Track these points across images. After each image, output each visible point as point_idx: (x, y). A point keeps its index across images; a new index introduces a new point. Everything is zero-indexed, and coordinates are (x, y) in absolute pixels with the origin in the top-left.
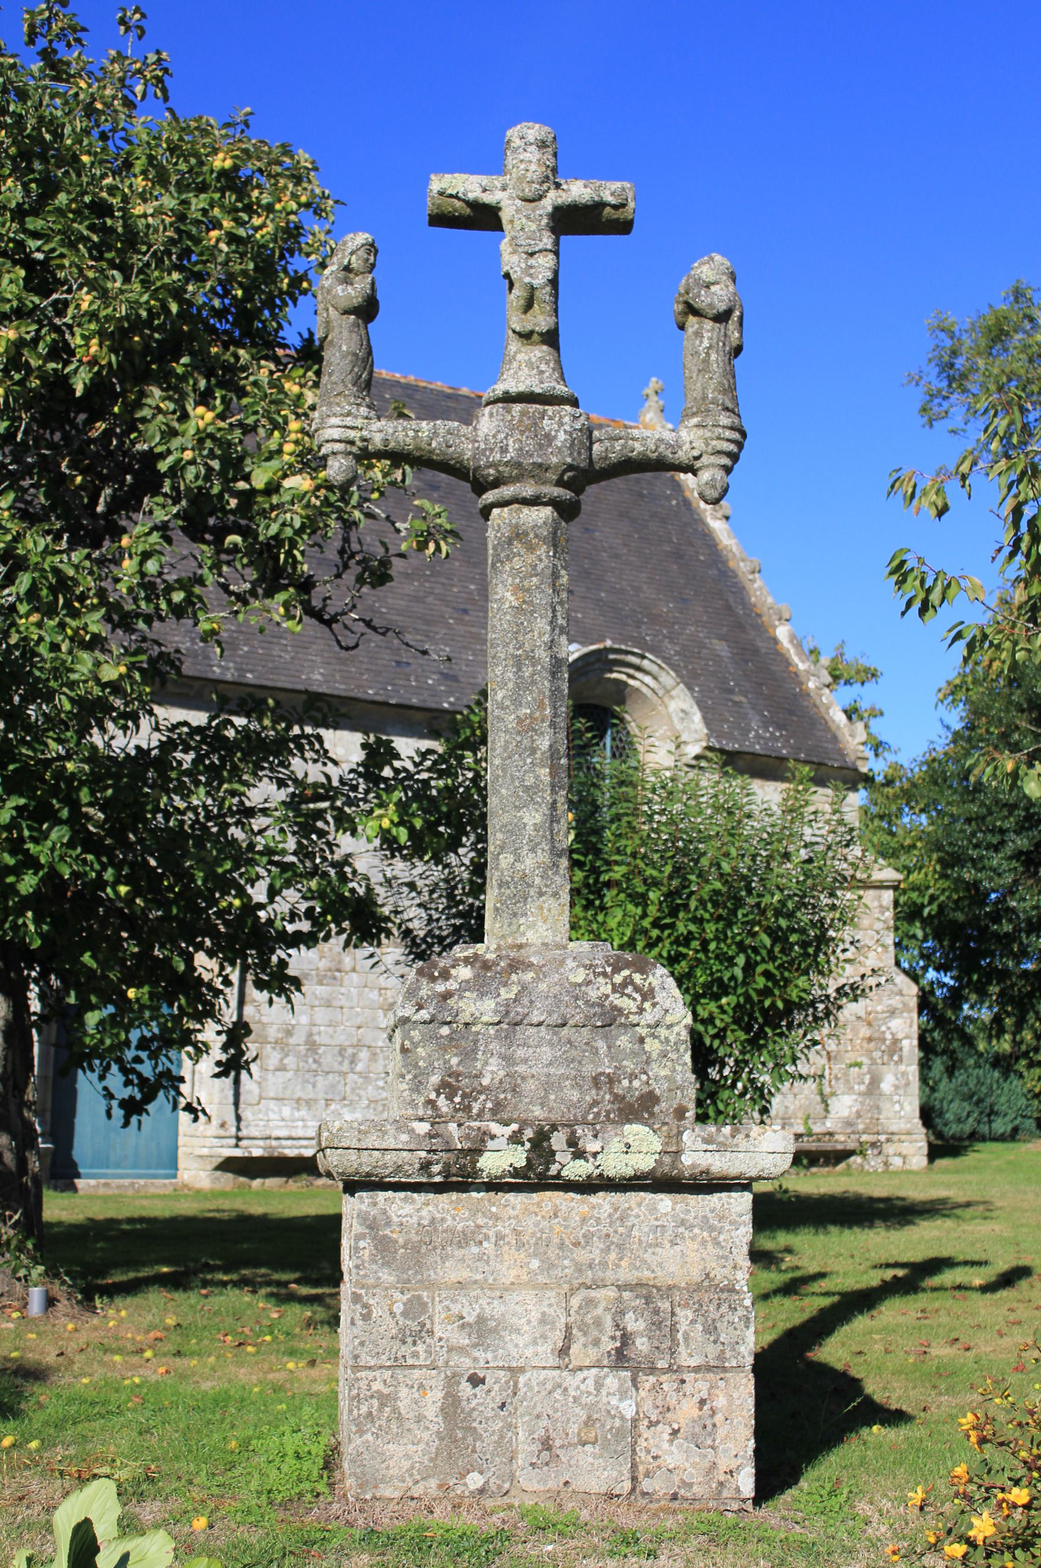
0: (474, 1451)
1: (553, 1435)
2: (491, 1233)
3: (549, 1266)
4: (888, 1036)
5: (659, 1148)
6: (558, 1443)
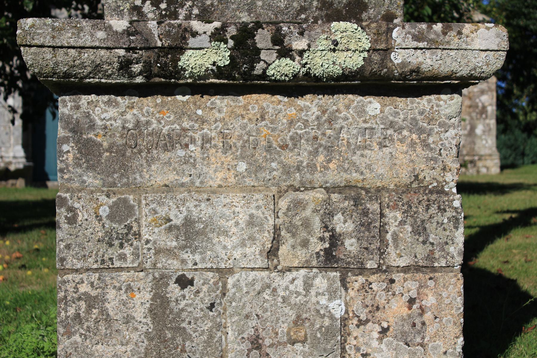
0: (183, 351)
1: (263, 334)
2: (197, 136)
3: (256, 169)
4: (480, 105)
5: (368, 46)
6: (267, 342)
